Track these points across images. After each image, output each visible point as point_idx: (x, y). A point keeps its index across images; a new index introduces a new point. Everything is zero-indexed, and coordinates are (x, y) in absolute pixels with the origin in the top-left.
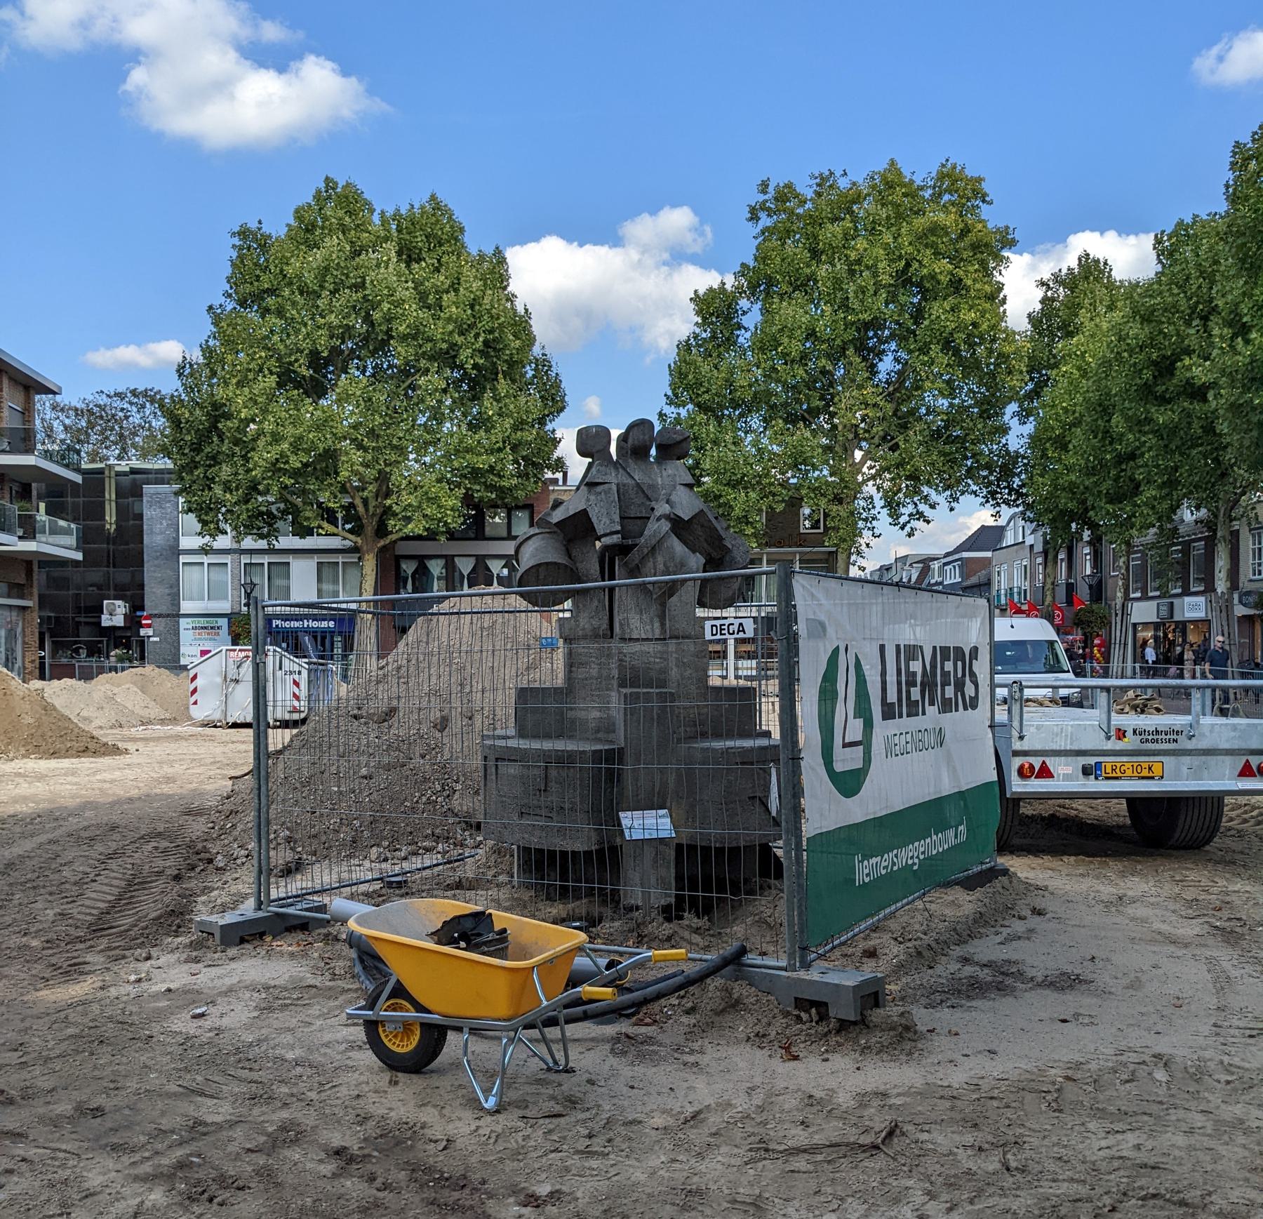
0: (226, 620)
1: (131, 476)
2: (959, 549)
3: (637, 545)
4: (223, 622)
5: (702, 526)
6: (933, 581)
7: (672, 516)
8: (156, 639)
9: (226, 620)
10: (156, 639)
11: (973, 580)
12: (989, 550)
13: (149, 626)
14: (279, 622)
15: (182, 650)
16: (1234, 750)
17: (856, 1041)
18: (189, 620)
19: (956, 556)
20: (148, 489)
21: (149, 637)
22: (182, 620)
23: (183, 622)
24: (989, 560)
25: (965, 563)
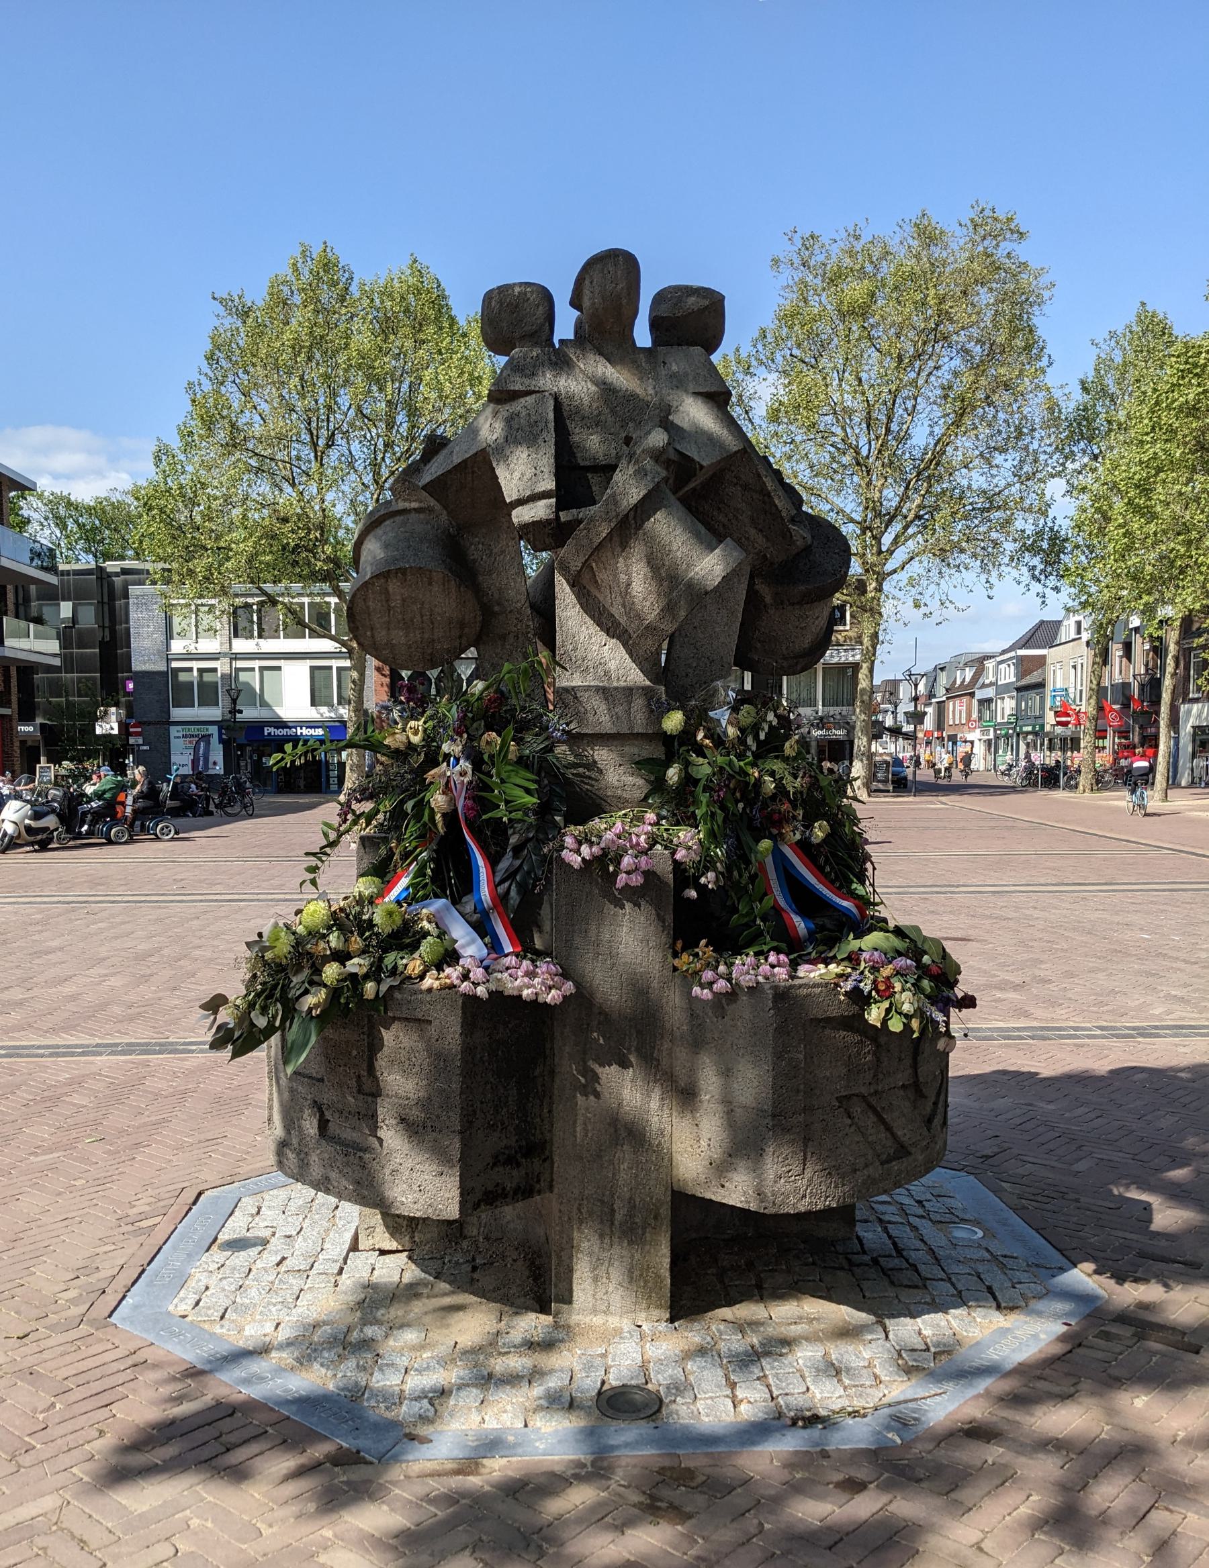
0: (216, 728)
1: (123, 577)
2: (1012, 648)
3: (580, 522)
4: (213, 730)
5: (745, 487)
6: (987, 682)
7: (672, 455)
8: (145, 748)
9: (216, 728)
10: (145, 748)
11: (1029, 680)
12: (1045, 647)
13: (137, 734)
14: (272, 730)
15: (174, 759)
16: (115, 615)
17: (650, 593)
18: (179, 728)
19: (1012, 654)
20: (134, 590)
21: (139, 745)
22: (172, 728)
23: (174, 730)
24: (1044, 657)
25: (1021, 660)
